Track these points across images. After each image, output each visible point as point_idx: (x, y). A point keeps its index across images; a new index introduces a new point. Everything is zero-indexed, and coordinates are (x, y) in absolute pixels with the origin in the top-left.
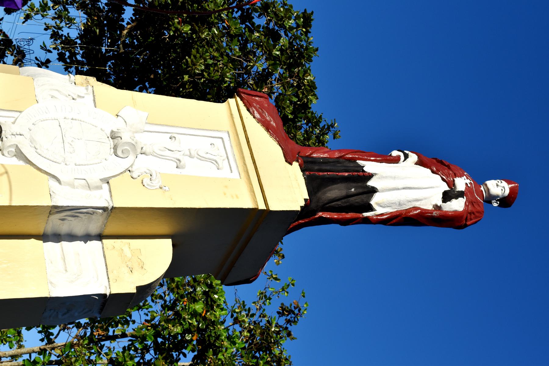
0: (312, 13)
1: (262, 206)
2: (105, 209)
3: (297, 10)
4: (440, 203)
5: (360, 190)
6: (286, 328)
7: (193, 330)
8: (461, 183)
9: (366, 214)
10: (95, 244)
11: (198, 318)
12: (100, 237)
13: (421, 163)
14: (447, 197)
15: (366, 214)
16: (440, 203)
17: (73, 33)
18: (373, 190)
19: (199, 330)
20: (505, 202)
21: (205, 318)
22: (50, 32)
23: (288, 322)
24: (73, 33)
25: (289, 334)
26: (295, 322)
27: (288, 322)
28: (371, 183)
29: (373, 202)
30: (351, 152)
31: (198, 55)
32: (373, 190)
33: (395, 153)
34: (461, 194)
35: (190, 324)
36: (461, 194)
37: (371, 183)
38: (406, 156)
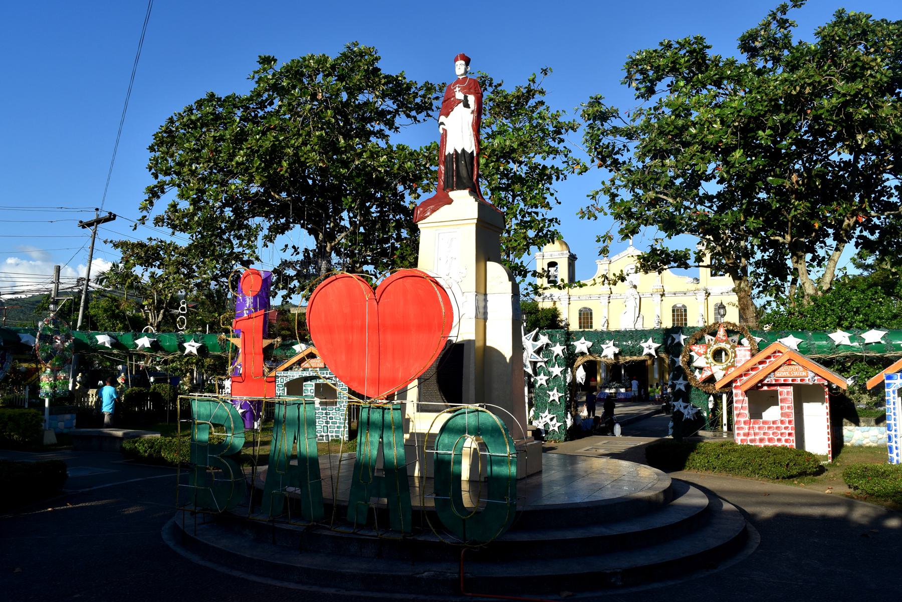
0: (260, 56)
1: (475, 221)
2: (476, 295)
3: (259, 67)
4: (470, 110)
5: (463, 158)
6: (495, 86)
7: (497, 166)
8: (459, 96)
9: (475, 155)
10: (489, 297)
11: (489, 161)
12: (485, 294)
13: (447, 115)
14: (467, 105)
15: (475, 155)
16: (470, 110)
17: (266, 225)
18: (463, 150)
19: (498, 160)
20: (468, 62)
21: (490, 156)
22: (269, 244)
23: (490, 85)
24: (266, 225)
25: (500, 85)
26: (491, 80)
27: (490, 85)
28: (459, 151)
29: (470, 152)
30: (602, 451)
31: (305, 156)
32: (463, 150)
33: (441, 131)
34: (466, 97)
35: (493, 168)
36: (466, 97)
37: (459, 151)
38: (442, 123)
